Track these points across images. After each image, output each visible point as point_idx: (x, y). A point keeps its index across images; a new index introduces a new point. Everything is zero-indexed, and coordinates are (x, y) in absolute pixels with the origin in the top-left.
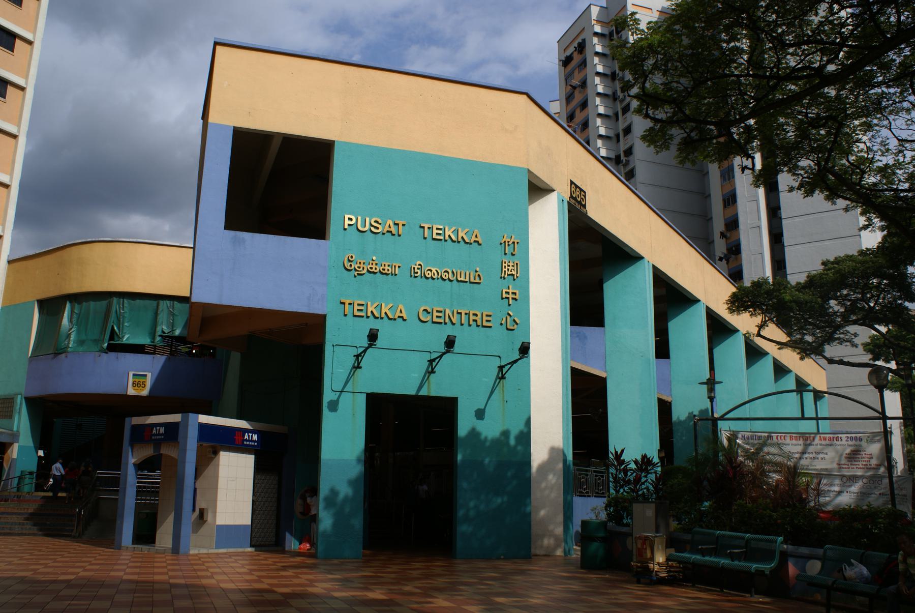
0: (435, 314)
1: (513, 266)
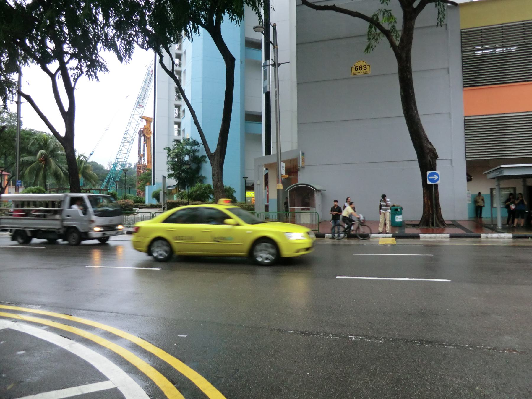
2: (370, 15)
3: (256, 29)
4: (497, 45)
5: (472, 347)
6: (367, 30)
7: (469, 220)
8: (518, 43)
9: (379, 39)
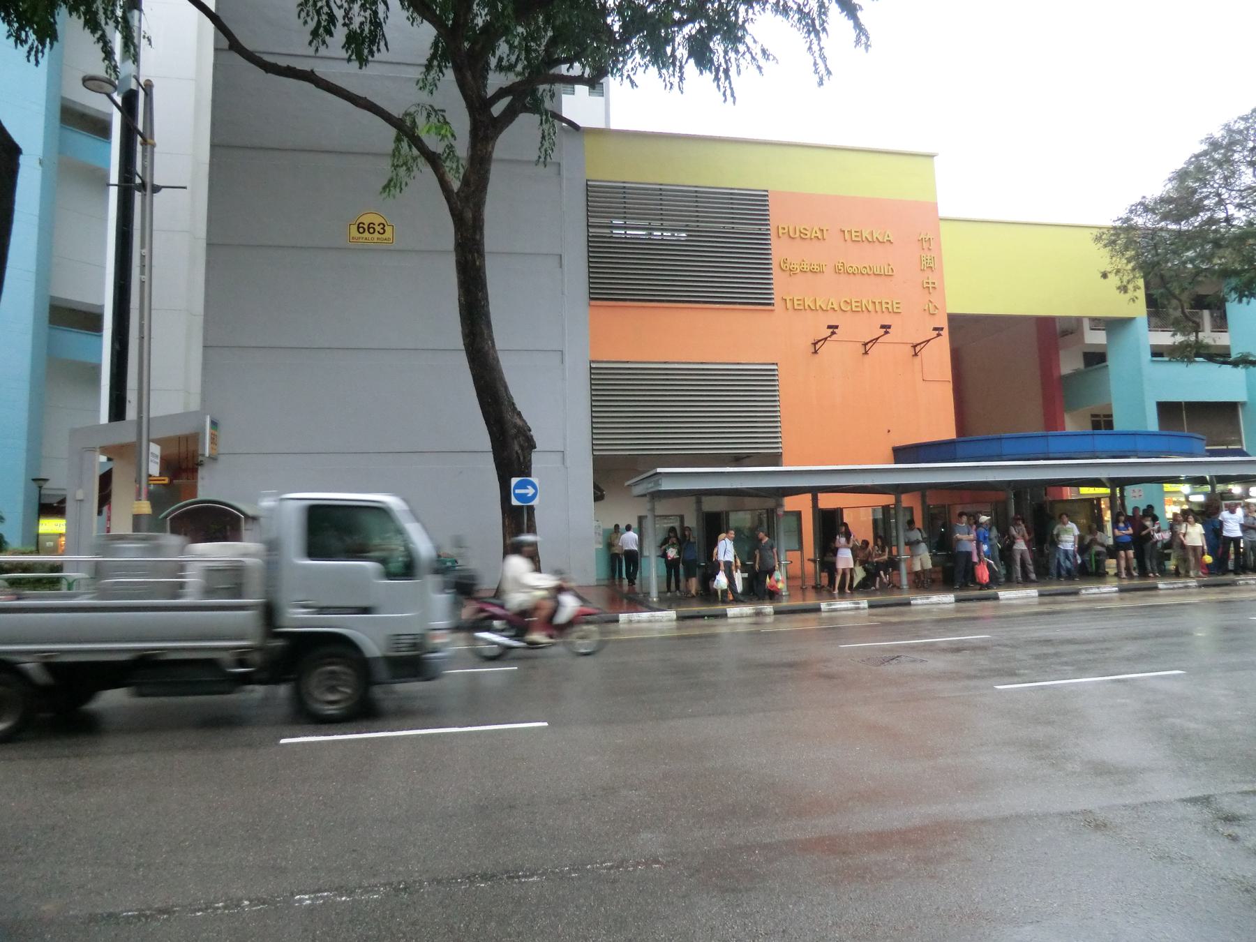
0: (854, 304)
1: (931, 259)
2: (397, 112)
3: (89, 83)
4: (653, 223)
5: (575, 871)
6: (391, 146)
7: (597, 586)
8: (687, 226)
9: (415, 168)
